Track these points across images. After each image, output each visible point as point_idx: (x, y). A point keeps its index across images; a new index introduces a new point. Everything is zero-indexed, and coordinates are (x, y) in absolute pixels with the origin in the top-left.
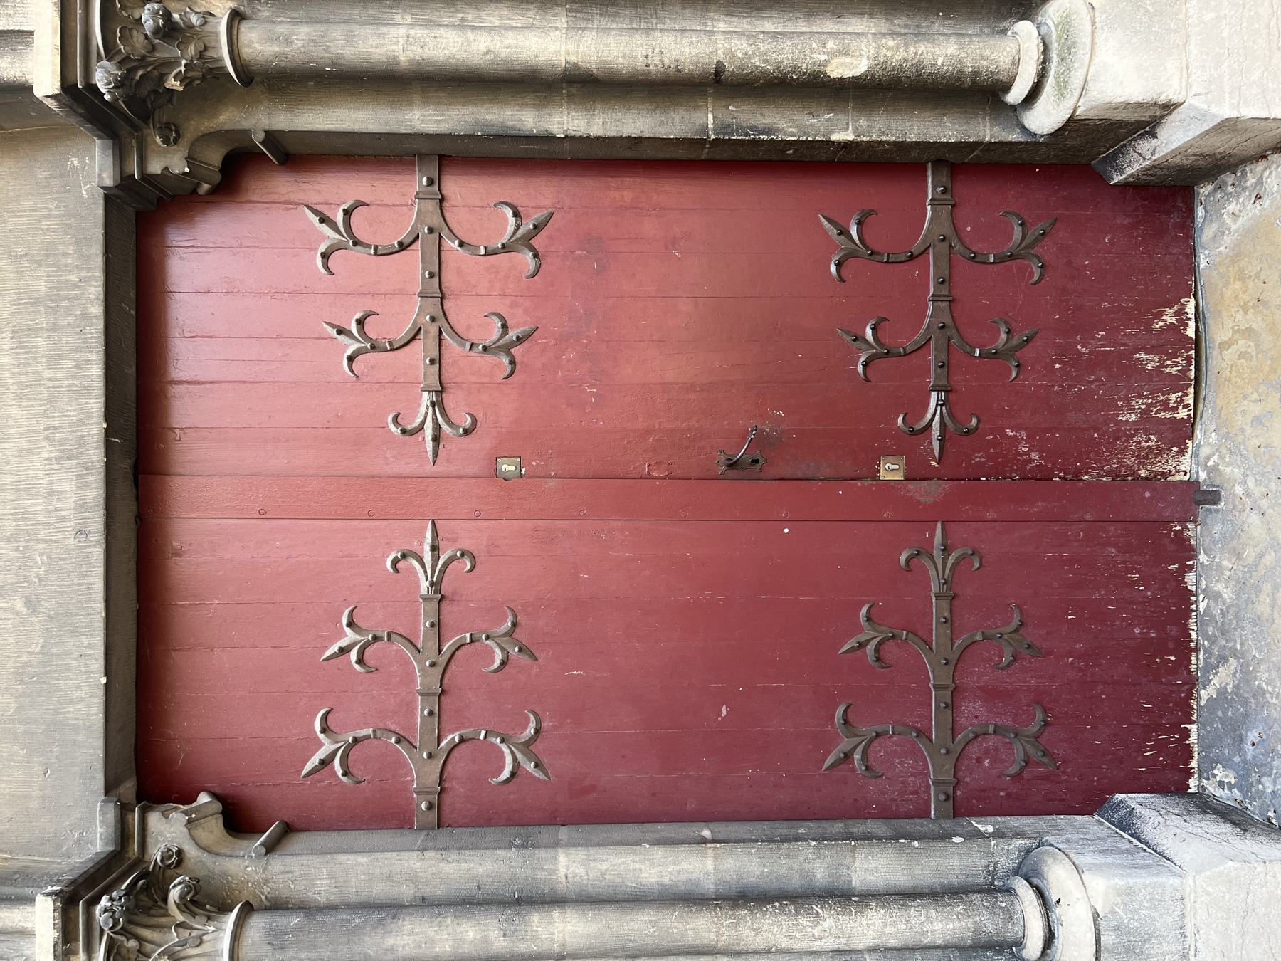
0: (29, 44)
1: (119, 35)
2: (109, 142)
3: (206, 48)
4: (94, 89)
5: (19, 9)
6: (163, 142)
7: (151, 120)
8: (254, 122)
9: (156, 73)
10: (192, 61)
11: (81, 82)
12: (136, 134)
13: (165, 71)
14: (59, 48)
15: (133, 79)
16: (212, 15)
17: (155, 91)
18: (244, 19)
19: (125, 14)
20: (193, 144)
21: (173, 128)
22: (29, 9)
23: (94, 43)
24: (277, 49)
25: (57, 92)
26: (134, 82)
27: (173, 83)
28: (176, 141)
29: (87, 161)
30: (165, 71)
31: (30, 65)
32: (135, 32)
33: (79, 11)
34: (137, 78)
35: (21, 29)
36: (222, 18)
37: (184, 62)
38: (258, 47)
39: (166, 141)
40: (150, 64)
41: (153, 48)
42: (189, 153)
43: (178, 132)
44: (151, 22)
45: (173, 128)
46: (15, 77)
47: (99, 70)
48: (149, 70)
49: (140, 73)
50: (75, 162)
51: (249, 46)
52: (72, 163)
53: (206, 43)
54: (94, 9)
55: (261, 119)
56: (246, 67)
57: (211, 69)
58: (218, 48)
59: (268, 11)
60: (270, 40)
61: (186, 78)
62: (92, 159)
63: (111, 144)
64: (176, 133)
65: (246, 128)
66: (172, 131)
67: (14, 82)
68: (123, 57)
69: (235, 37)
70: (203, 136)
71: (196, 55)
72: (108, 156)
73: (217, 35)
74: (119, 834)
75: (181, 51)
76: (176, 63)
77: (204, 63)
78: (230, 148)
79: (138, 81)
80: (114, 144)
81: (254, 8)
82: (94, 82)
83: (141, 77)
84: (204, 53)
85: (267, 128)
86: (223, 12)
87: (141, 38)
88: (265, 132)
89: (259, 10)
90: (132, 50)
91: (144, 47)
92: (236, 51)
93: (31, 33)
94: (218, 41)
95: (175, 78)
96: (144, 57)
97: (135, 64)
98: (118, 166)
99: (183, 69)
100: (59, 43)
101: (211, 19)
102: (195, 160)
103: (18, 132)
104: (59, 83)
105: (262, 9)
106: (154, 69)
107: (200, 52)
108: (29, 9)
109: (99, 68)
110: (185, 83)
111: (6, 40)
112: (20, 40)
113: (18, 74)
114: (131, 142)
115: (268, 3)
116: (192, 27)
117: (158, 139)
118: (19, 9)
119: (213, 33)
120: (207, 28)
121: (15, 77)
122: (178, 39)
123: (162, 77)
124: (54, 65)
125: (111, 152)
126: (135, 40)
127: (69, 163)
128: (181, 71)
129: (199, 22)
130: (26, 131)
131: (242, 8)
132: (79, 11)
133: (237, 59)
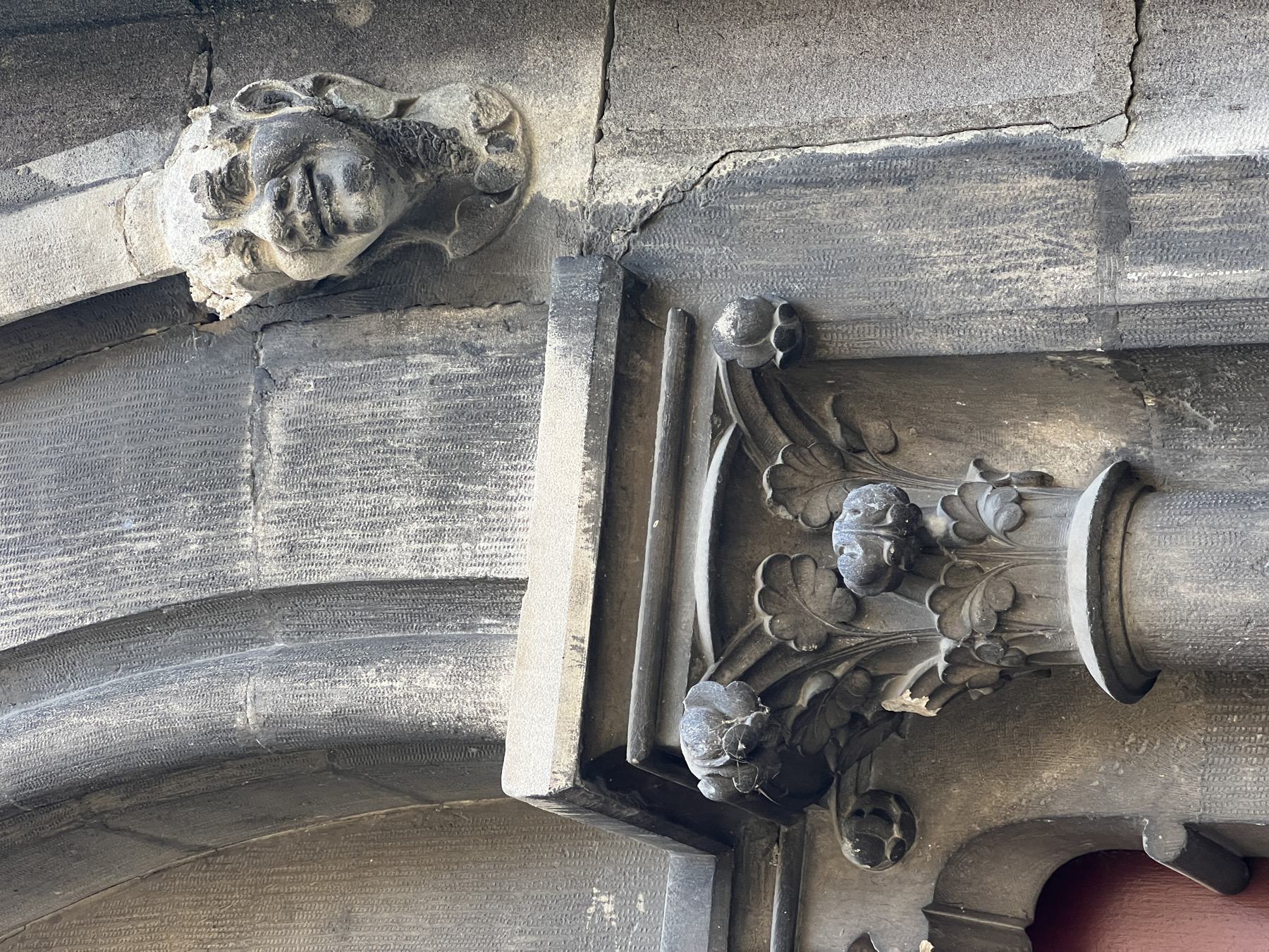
0: (509, 612)
1: (760, 585)
2: (705, 863)
3: (1017, 601)
4: (674, 759)
5: (492, 515)
6: (862, 858)
7: (833, 788)
8: (1151, 793)
9: (860, 679)
10: (971, 640)
11: (637, 745)
12: (784, 829)
13: (883, 668)
14: (586, 645)
15: (792, 705)
16: (1044, 480)
17: (856, 717)
18: (1150, 489)
19: (783, 513)
20: (951, 861)
21: (896, 811)
22: (519, 515)
23: (685, 619)
24: (1252, 598)
25: (563, 783)
26: (794, 713)
27: (903, 700)
28: (900, 851)
29: (641, 907)
30: (883, 668)
31: (502, 685)
32: (808, 569)
33: (653, 524)
34: (803, 701)
35: (493, 574)
36: (1078, 492)
37: (945, 645)
38: (1187, 592)
39: (872, 853)
40: (845, 655)
41: (859, 608)
42: (937, 892)
43: (909, 827)
44: (859, 551)
45: (896, 811)
46: (459, 718)
47: (691, 712)
48: (838, 673)
49: (811, 688)
50: (608, 908)
51: (1157, 591)
52: (599, 910)
53: (1020, 584)
54: (694, 536)
55: (1174, 783)
56: (1143, 650)
57: (1032, 656)
58: (1056, 595)
59: (1229, 457)
60: (1230, 569)
61: (945, 686)
62: (654, 903)
63: (710, 868)
64: (902, 828)
65: (1126, 811)
66: (890, 822)
67: (456, 730)
68: (769, 646)
69: (1114, 565)
70: (984, 834)
71: (985, 624)
72: (697, 905)
73: (1056, 557)
74: (662, 717)
75: (942, 614)
76: (925, 645)
77: (1006, 647)
78: (1066, 857)
79: (804, 713)
80: (718, 867)
81: (1181, 449)
82: (671, 741)
83: (815, 699)
84: (1015, 617)
85: (1195, 816)
86: (1082, 466)
87: (827, 582)
88: (1189, 827)
89: (1198, 455)
90: (796, 626)
91: (831, 611)
92: (1114, 609)
93: (521, 584)
94: (1057, 578)
95: (915, 690)
96: (830, 638)
97: (800, 663)
98: (723, 938)
99: (942, 665)
100: (585, 633)
101: (1040, 502)
102: (956, 910)
103: (466, 810)
104: (574, 756)
105: (1213, 450)
106: (857, 668)
107: (999, 614)
108: (519, 515)
109: (690, 704)
110: (942, 699)
111: (450, 602)
112: (486, 601)
113: (469, 710)
114: (768, 850)
115: (1228, 433)
116: (980, 537)
117: (847, 847)
118: (492, 515)
119: (1043, 552)
120: (1030, 536)
121: (459, 718)
122: (934, 579)
123: (877, 685)
124: (564, 699)
125: (708, 890)
126: (806, 590)
127: (592, 910)
128: (934, 669)
129: (1003, 517)
130: (487, 807)
131: (1143, 453)
132: (653, 524)
133: (1114, 630)
